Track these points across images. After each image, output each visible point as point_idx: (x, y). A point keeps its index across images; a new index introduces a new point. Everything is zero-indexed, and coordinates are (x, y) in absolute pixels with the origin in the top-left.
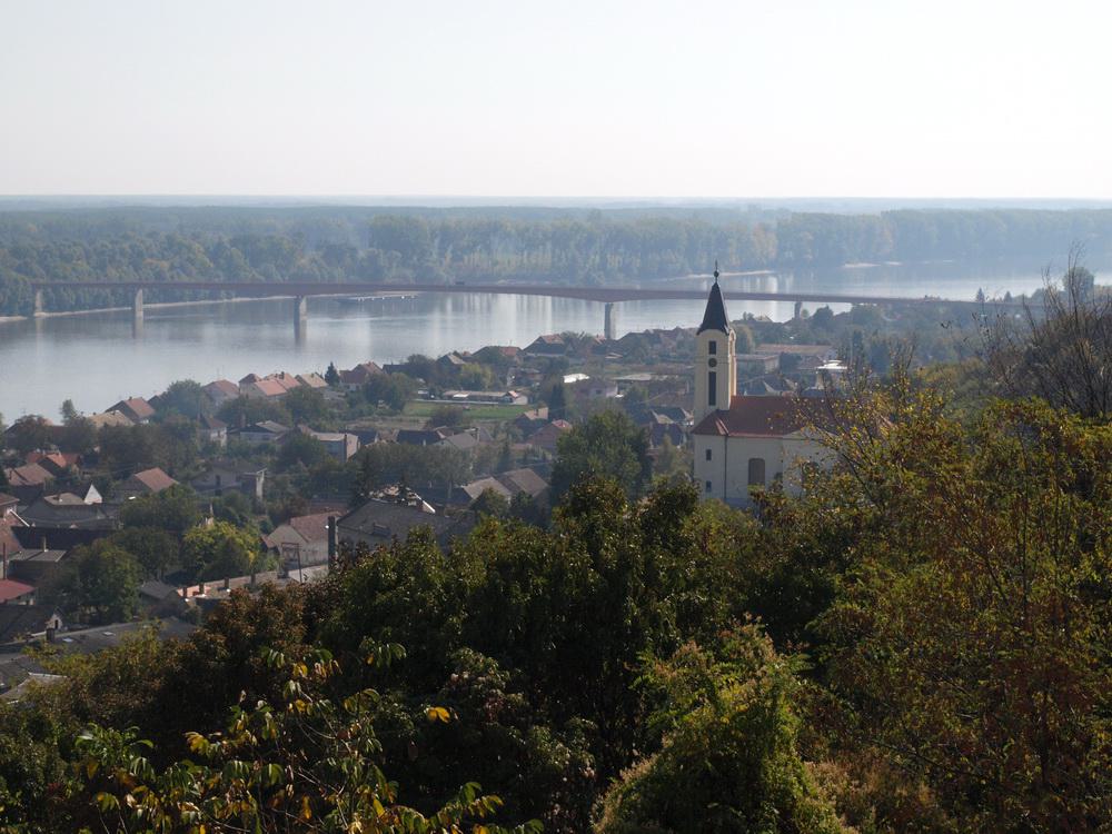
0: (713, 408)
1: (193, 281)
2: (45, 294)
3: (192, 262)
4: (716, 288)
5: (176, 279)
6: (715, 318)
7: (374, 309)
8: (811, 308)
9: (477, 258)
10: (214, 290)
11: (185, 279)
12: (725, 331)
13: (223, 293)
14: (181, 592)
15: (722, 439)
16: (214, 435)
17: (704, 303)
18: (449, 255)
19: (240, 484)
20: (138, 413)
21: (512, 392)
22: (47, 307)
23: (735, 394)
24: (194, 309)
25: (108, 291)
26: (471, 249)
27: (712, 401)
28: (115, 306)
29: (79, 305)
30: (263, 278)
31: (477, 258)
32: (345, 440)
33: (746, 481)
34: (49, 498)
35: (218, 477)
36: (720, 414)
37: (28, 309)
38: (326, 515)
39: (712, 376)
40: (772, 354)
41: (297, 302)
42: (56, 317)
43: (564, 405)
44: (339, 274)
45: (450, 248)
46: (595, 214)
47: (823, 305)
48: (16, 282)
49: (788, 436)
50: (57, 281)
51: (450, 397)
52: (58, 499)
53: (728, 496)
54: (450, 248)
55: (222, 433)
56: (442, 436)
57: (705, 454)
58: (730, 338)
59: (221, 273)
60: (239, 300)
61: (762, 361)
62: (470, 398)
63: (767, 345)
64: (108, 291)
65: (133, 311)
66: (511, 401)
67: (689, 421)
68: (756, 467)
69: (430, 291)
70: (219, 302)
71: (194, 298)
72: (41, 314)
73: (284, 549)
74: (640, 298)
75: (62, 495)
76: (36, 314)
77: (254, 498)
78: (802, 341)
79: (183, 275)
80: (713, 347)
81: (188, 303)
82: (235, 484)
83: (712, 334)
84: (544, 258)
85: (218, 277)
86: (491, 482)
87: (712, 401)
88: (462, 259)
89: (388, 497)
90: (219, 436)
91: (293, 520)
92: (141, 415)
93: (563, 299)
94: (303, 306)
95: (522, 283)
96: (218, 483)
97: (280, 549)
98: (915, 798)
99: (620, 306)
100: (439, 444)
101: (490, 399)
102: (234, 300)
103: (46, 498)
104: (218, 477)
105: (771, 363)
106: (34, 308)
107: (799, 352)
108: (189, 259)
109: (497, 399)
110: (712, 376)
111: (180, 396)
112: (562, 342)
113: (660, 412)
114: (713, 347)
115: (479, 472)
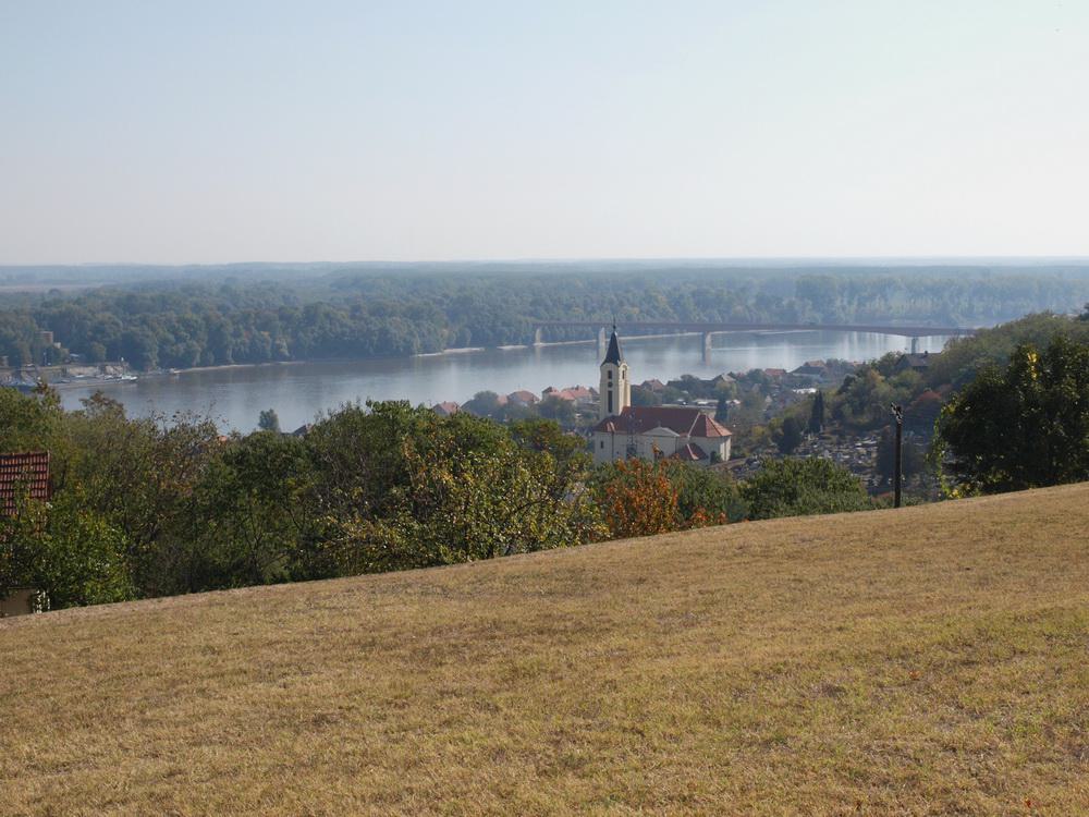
0: (610, 415)
1: (655, 321)
2: (543, 331)
3: (656, 308)
5: (642, 321)
7: (792, 340)
9: (878, 304)
10: (670, 328)
11: (649, 320)
18: (856, 303)
22: (544, 339)
23: (629, 405)
24: (655, 340)
25: (590, 328)
26: (872, 298)
27: (610, 410)
29: (567, 338)
30: (707, 320)
31: (878, 304)
36: (614, 419)
37: (529, 341)
39: (610, 393)
41: (704, 337)
42: (550, 347)
43: (792, 419)
44: (765, 317)
45: (857, 297)
46: (985, 271)
48: (520, 322)
49: (647, 433)
50: (553, 322)
51: (696, 404)
54: (857, 297)
57: (605, 445)
59: (675, 316)
60: (690, 334)
62: (708, 404)
64: (590, 328)
65: (598, 343)
68: (631, 451)
69: (833, 329)
70: (673, 335)
71: (655, 333)
72: (539, 344)
74: (929, 334)
76: (536, 344)
79: (649, 318)
81: (651, 337)
84: (926, 304)
85: (673, 318)
87: (610, 410)
88: (865, 306)
93: (882, 335)
94: (708, 339)
95: (908, 323)
102: (686, 334)
106: (534, 340)
108: (654, 307)
110: (610, 393)
111: (483, 401)
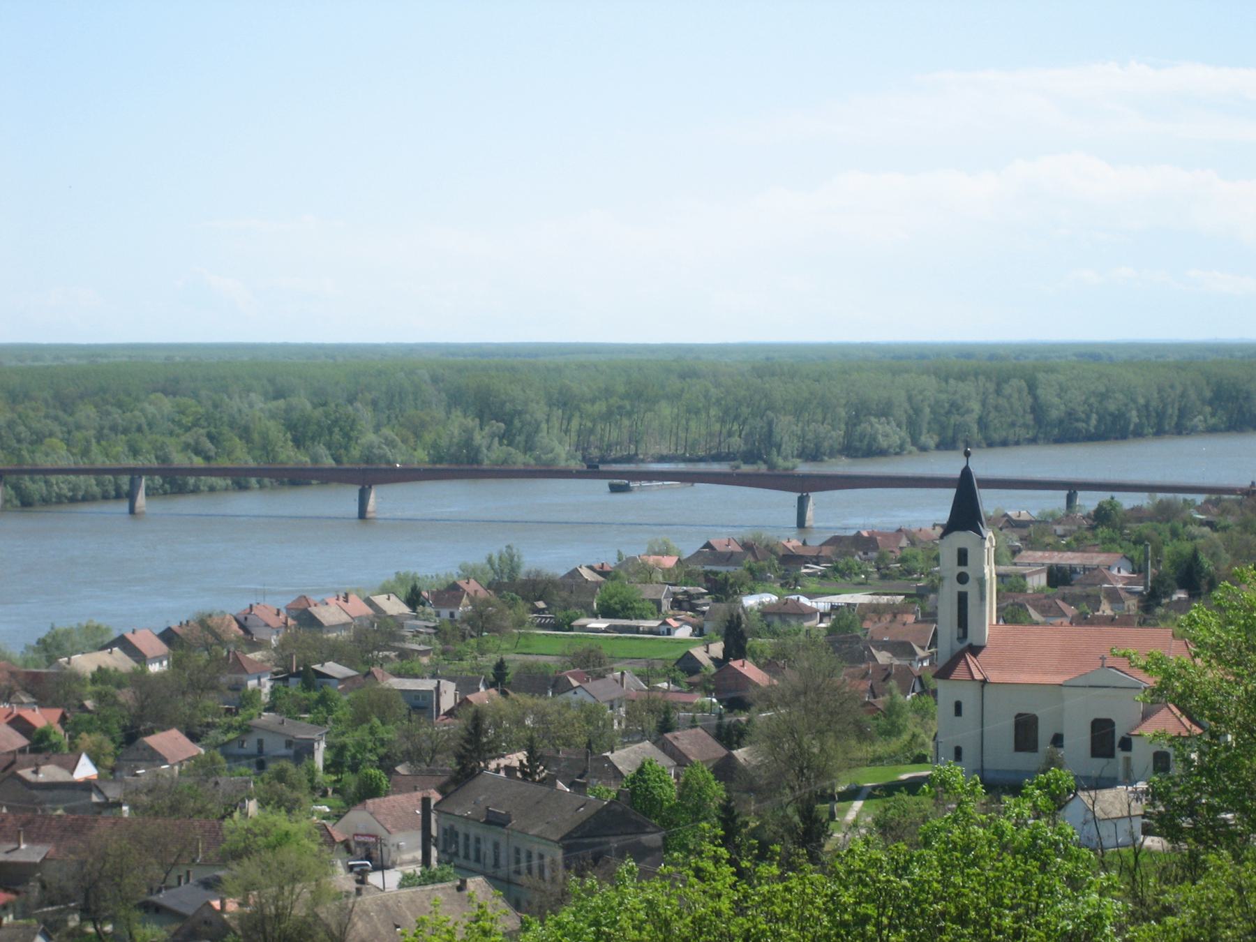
4: (966, 473)
6: (966, 515)
8: (1088, 502)
12: (980, 533)
13: (253, 481)
14: (216, 904)
15: (978, 686)
16: (252, 683)
17: (951, 493)
19: (291, 752)
20: (143, 650)
21: (670, 621)
28: (1001, 577)
32: (438, 689)
33: (1012, 745)
34: (27, 773)
35: (260, 742)
38: (419, 795)
39: (962, 599)
40: (1036, 564)
47: (1104, 496)
51: (583, 628)
52: (36, 772)
53: (986, 766)
55: (263, 680)
56: (575, 683)
57: (952, 709)
58: (987, 544)
61: (1024, 576)
63: (1030, 553)
66: (669, 633)
67: (922, 660)
73: (358, 843)
75: (43, 768)
77: (311, 773)
78: (1078, 544)
80: (962, 557)
82: (283, 751)
83: (962, 539)
86: (646, 748)
89: (509, 770)
90: (259, 684)
91: (369, 802)
92: (149, 654)
96: (260, 750)
97: (353, 844)
98: (82, 920)
99: (814, 498)
100: (570, 694)
101: (636, 630)
103: (20, 772)
104: (260, 742)
105: (1036, 578)
107: (1075, 562)
109: (651, 631)
110: (962, 599)
112: (739, 549)
113: (883, 646)
114: (962, 557)
115: (629, 737)
